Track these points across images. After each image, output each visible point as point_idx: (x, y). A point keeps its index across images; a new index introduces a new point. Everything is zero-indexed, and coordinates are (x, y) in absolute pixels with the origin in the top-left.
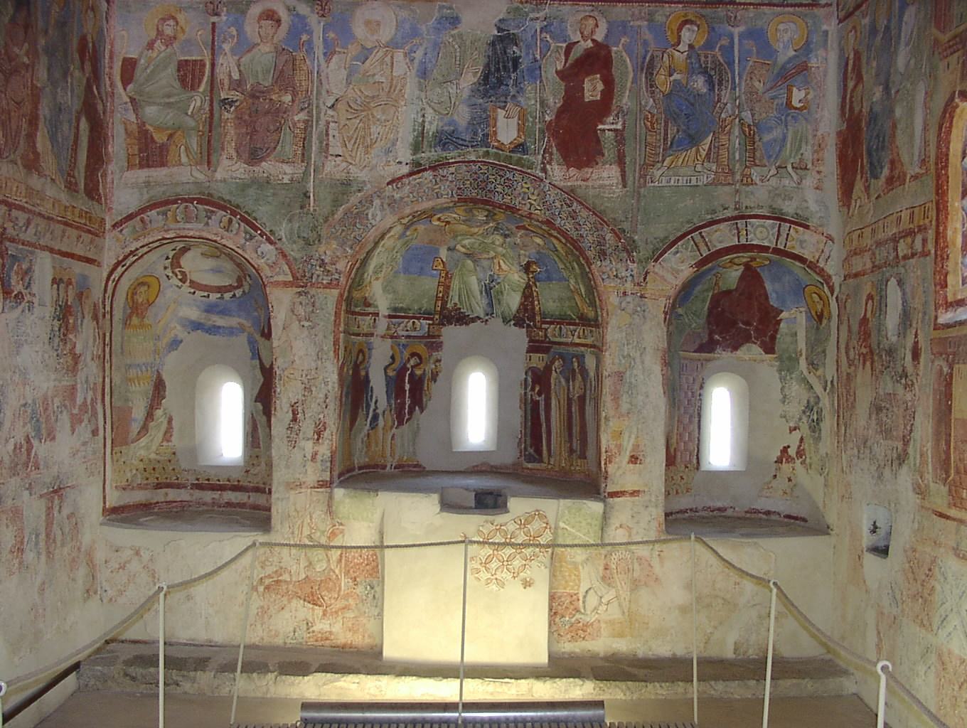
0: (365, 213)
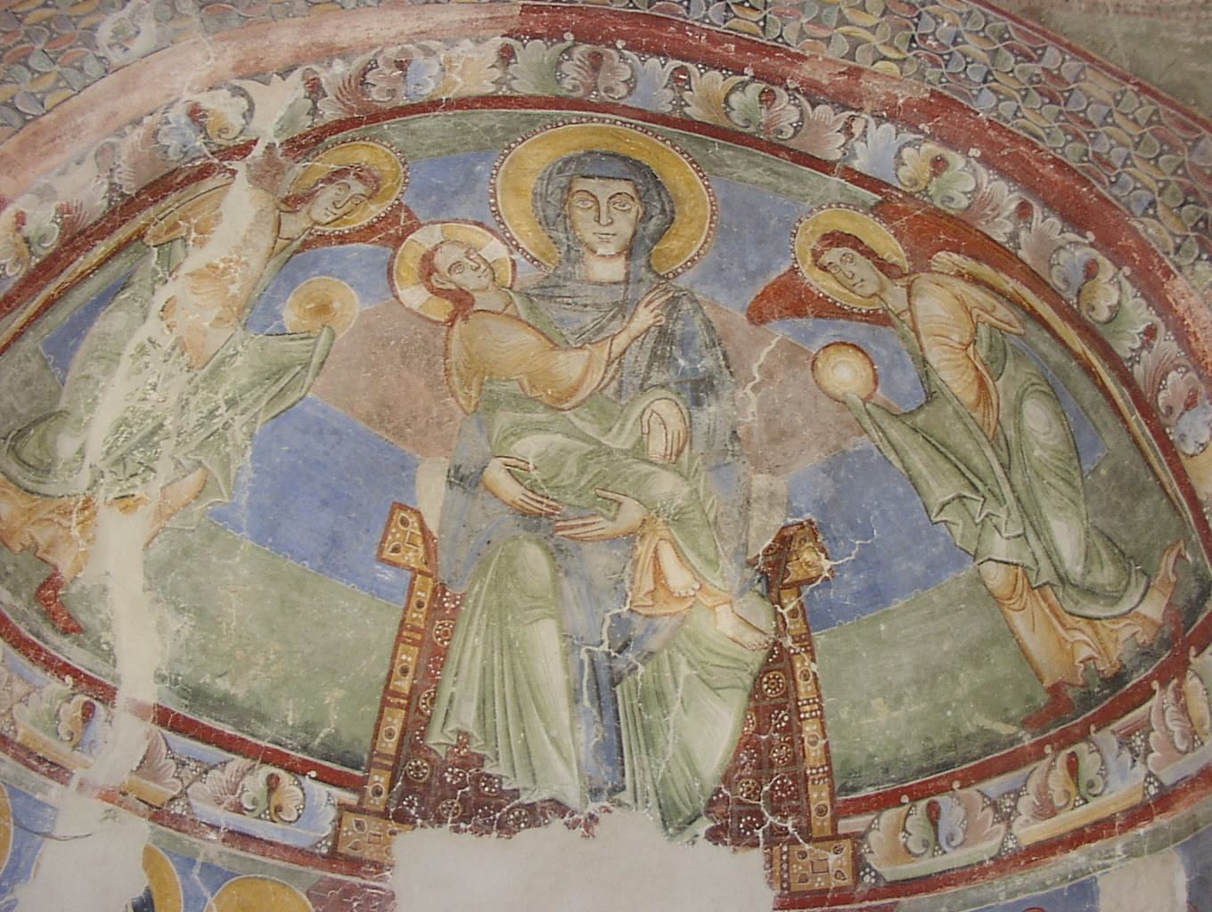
0: (84, 23)
